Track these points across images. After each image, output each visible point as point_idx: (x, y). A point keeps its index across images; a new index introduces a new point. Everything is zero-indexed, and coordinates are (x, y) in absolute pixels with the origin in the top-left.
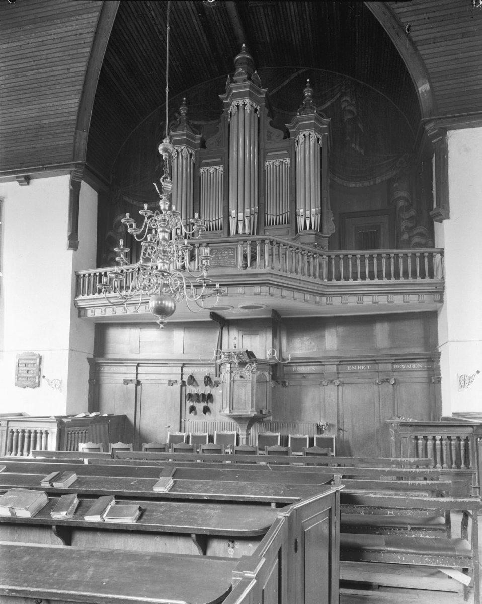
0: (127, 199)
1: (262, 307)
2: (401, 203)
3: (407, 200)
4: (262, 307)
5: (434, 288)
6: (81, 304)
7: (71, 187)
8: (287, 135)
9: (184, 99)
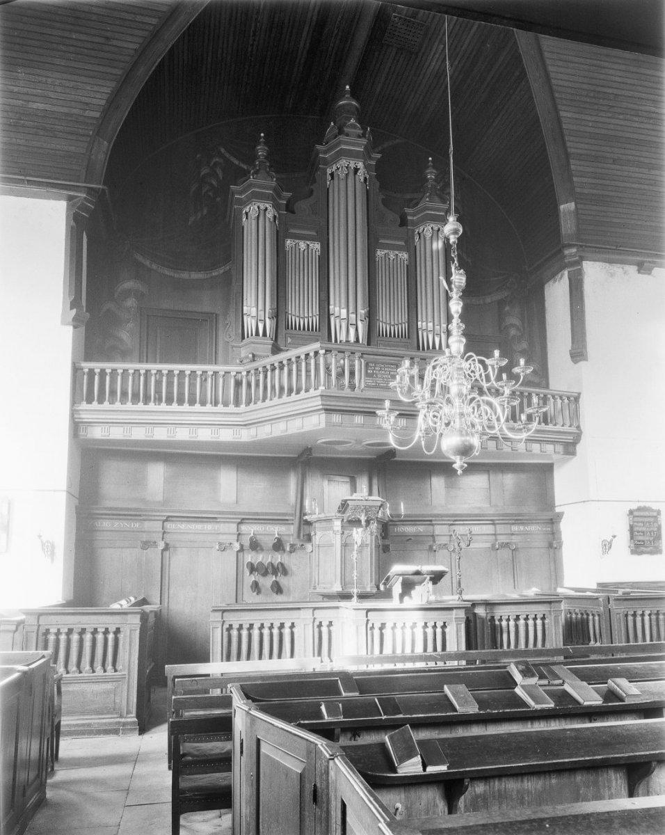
0: (140, 258)
1: (350, 443)
2: (513, 332)
3: (518, 329)
4: (350, 443)
5: (572, 438)
6: (85, 417)
7: (72, 223)
8: (403, 222)
9: (430, 159)
